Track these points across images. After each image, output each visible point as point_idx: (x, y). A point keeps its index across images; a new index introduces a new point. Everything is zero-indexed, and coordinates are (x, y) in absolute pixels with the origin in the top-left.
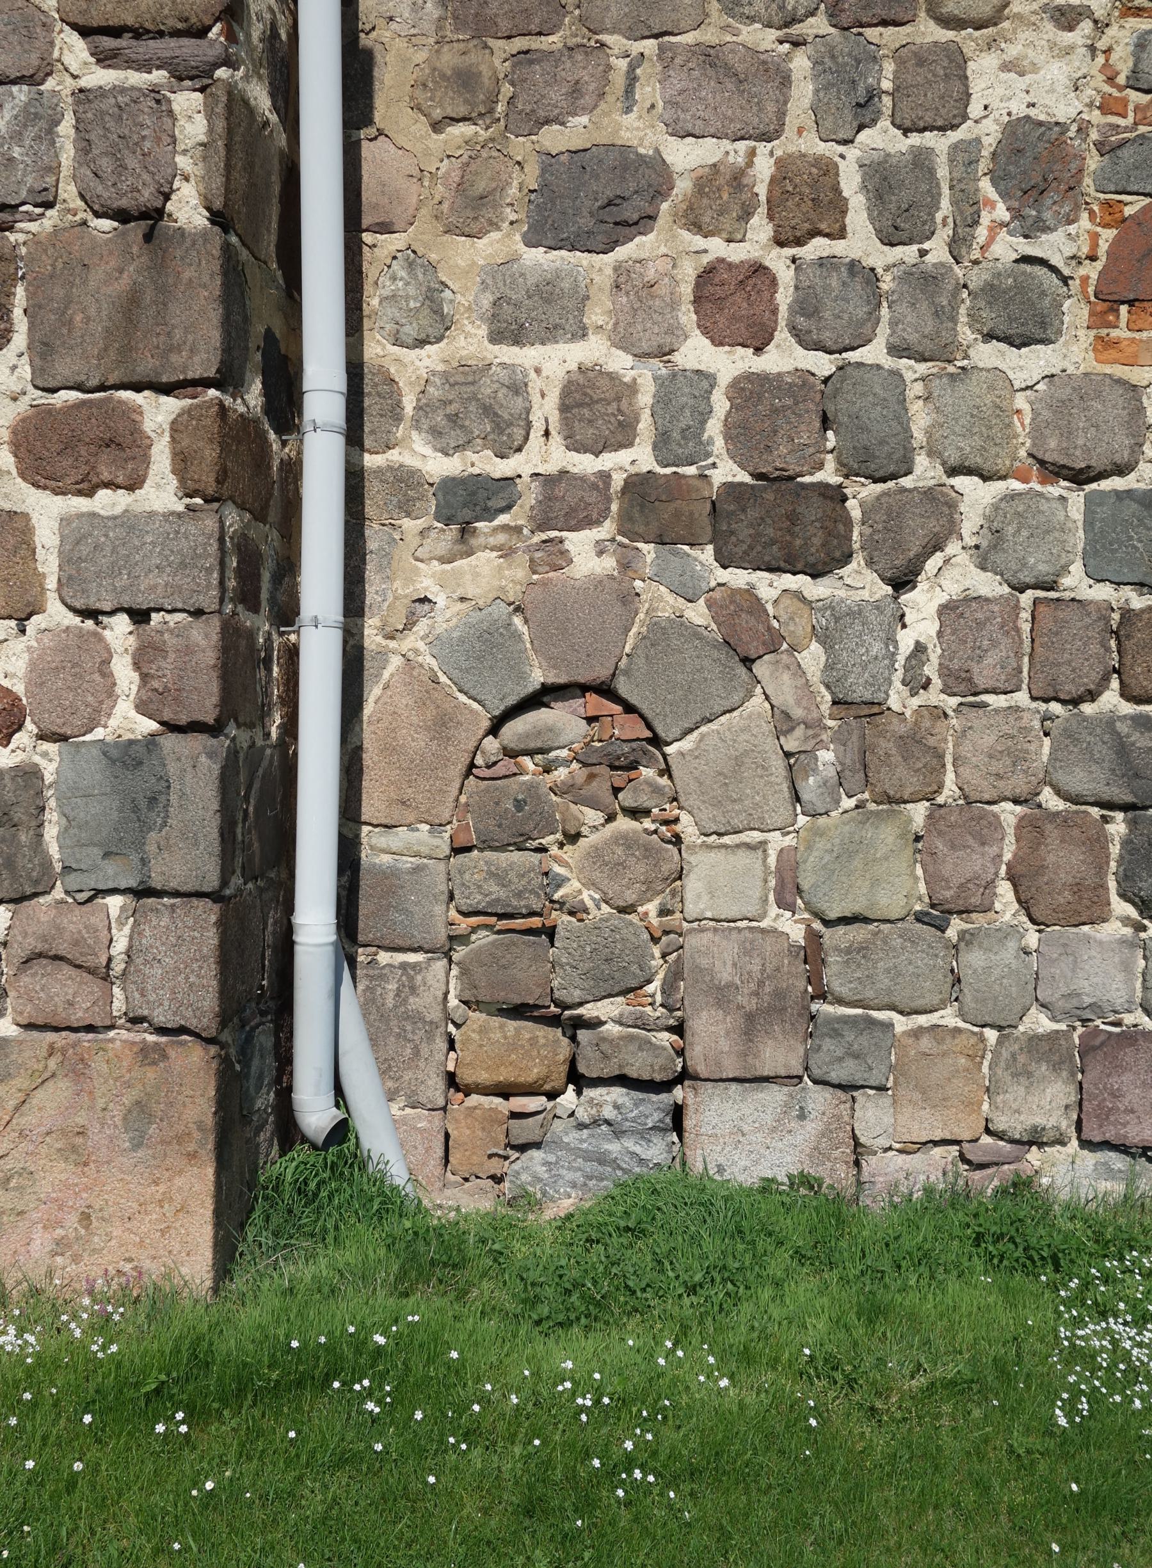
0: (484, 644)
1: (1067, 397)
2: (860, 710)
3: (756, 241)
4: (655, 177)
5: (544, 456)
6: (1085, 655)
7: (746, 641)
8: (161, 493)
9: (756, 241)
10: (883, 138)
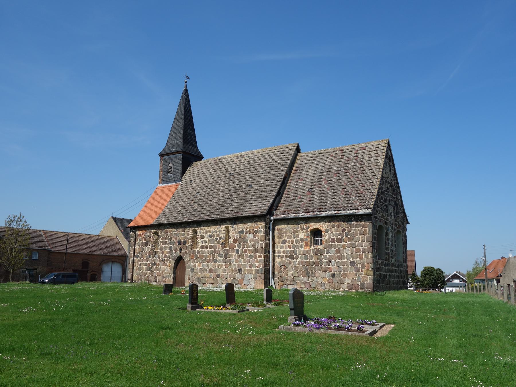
0: (280, 263)
1: (303, 251)
2: (295, 266)
3: (290, 244)
4: (286, 241)
5: (282, 254)
6: (304, 263)
7: (290, 263)
8: (262, 258)
9: (290, 244)
10: (296, 239)
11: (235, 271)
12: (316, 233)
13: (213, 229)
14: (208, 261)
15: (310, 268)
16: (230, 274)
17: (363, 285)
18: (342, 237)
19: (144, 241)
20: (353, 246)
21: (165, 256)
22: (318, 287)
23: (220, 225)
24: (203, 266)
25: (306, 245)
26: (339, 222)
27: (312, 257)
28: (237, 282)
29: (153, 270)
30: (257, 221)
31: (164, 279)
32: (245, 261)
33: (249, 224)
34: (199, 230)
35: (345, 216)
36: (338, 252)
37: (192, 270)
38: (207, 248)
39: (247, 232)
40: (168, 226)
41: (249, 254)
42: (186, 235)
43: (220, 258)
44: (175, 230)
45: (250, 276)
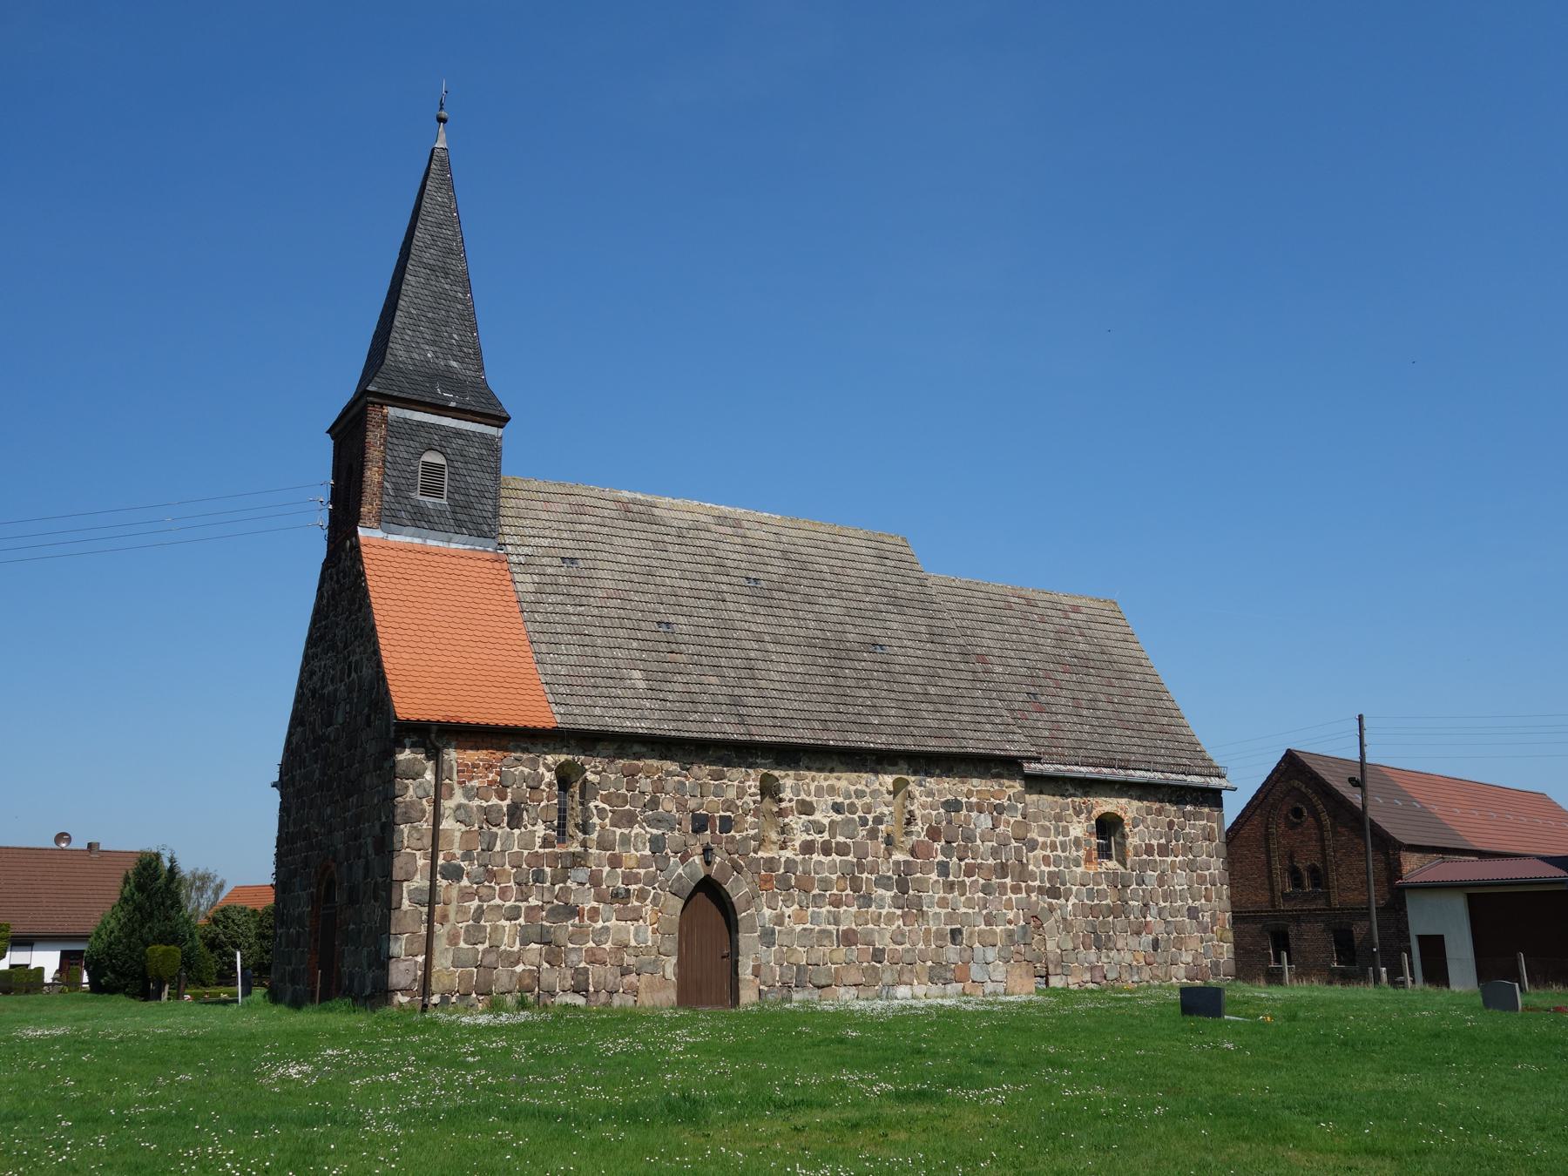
1: (1083, 874)
2: (1065, 919)
3: (1048, 852)
7: (1051, 909)
9: (1048, 852)
11: (940, 935)
12: (1108, 827)
13: (845, 781)
14: (836, 903)
15: (1104, 924)
16: (921, 946)
17: (1216, 965)
18: (1169, 842)
19: (494, 801)
20: (1191, 866)
21: (629, 878)
22: (1125, 976)
23: (876, 772)
24: (815, 918)
25: (1088, 860)
26: (1161, 801)
27: (1101, 894)
28: (949, 975)
29: (562, 937)
30: (999, 776)
31: (633, 978)
32: (970, 903)
33: (975, 781)
34: (788, 780)
35: (1182, 787)
36: (1161, 881)
37: (768, 937)
38: (827, 853)
39: (970, 808)
40: (636, 748)
41: (982, 881)
42: (731, 794)
43: (881, 891)
44: (673, 766)
45: (991, 954)
